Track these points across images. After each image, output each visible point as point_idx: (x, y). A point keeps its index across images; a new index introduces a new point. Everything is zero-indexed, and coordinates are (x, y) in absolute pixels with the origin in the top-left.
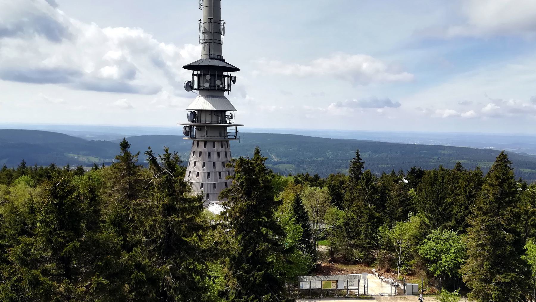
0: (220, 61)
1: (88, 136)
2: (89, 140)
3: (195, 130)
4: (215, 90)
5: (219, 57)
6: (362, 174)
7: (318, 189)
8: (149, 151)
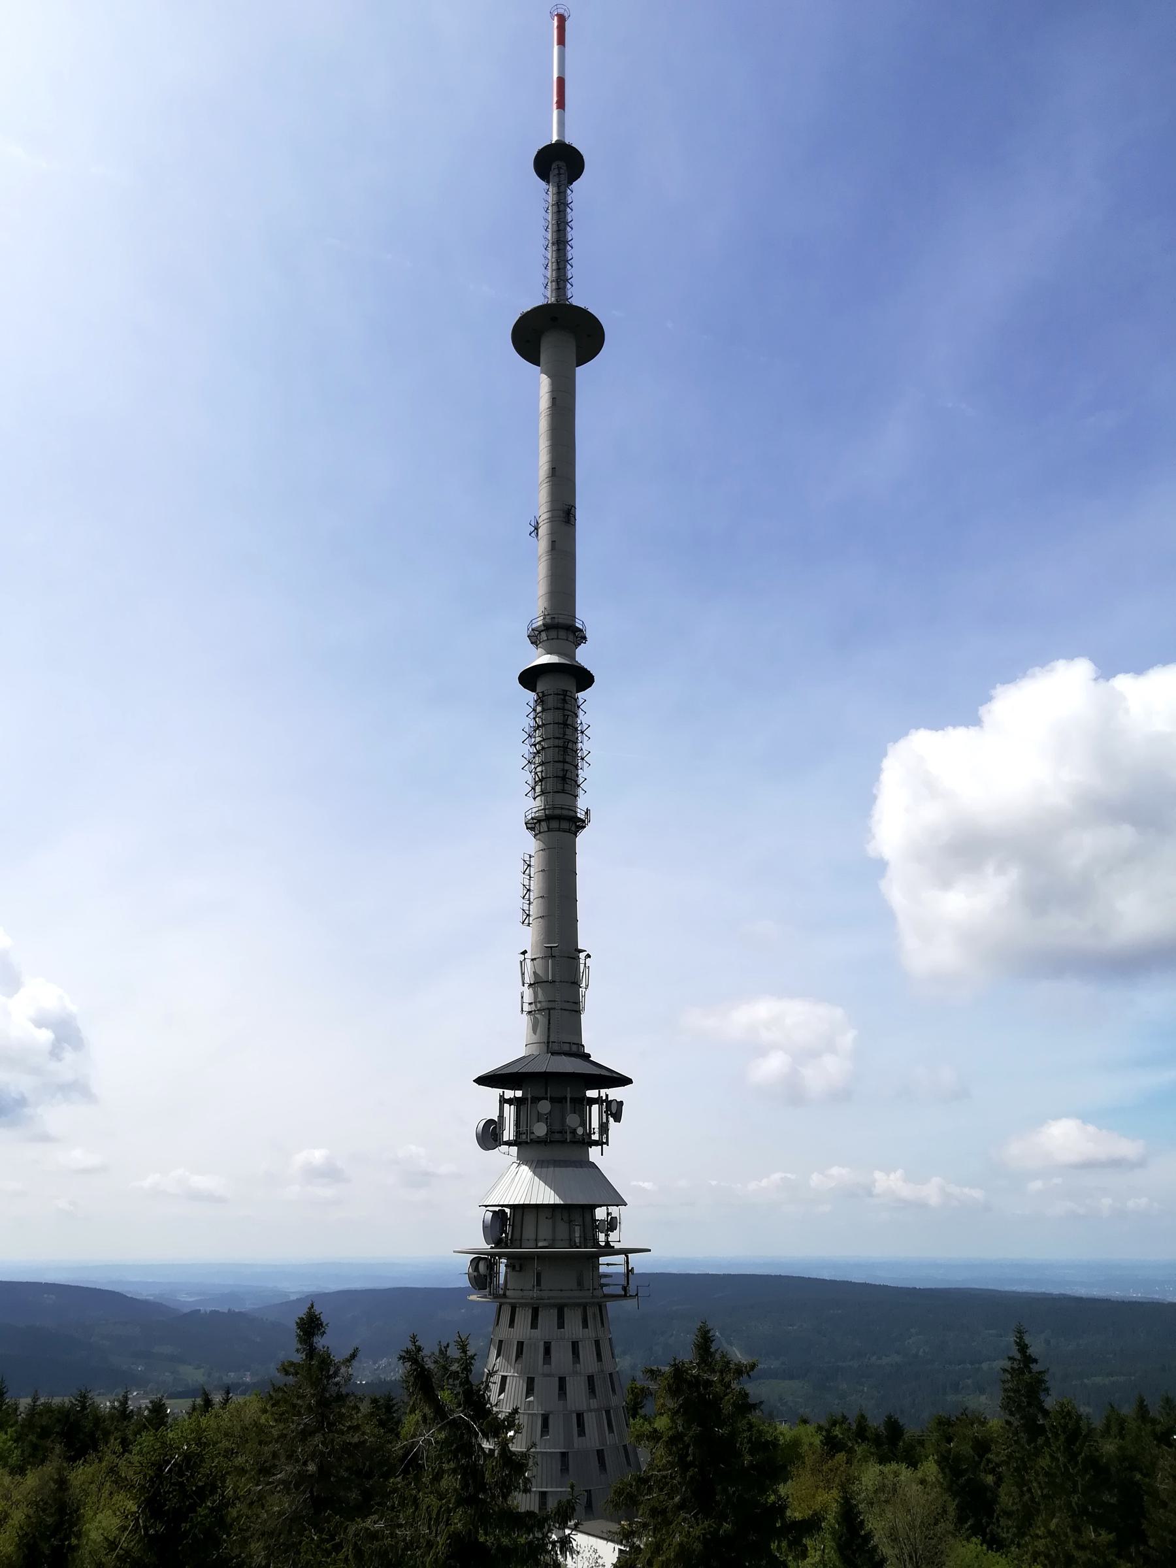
0: (578, 1061)
1: (183, 1298)
2: (186, 1310)
3: (503, 1268)
4: (564, 1142)
5: (574, 1048)
6: (1046, 1413)
7: (905, 1473)
8: (411, 1347)
